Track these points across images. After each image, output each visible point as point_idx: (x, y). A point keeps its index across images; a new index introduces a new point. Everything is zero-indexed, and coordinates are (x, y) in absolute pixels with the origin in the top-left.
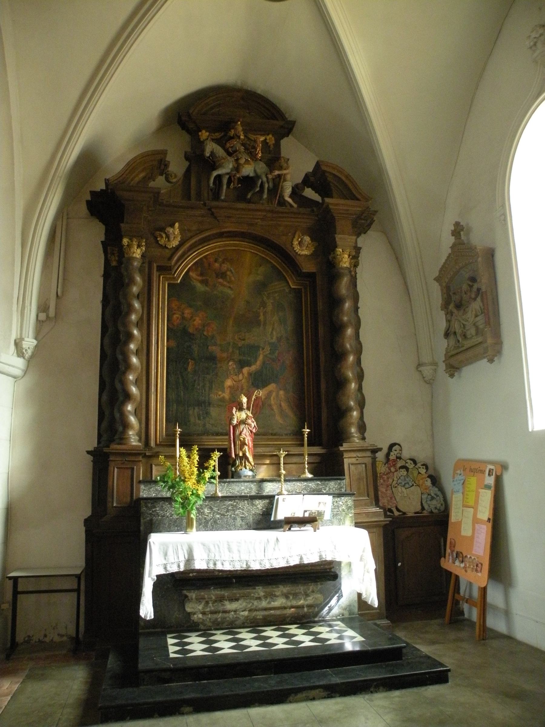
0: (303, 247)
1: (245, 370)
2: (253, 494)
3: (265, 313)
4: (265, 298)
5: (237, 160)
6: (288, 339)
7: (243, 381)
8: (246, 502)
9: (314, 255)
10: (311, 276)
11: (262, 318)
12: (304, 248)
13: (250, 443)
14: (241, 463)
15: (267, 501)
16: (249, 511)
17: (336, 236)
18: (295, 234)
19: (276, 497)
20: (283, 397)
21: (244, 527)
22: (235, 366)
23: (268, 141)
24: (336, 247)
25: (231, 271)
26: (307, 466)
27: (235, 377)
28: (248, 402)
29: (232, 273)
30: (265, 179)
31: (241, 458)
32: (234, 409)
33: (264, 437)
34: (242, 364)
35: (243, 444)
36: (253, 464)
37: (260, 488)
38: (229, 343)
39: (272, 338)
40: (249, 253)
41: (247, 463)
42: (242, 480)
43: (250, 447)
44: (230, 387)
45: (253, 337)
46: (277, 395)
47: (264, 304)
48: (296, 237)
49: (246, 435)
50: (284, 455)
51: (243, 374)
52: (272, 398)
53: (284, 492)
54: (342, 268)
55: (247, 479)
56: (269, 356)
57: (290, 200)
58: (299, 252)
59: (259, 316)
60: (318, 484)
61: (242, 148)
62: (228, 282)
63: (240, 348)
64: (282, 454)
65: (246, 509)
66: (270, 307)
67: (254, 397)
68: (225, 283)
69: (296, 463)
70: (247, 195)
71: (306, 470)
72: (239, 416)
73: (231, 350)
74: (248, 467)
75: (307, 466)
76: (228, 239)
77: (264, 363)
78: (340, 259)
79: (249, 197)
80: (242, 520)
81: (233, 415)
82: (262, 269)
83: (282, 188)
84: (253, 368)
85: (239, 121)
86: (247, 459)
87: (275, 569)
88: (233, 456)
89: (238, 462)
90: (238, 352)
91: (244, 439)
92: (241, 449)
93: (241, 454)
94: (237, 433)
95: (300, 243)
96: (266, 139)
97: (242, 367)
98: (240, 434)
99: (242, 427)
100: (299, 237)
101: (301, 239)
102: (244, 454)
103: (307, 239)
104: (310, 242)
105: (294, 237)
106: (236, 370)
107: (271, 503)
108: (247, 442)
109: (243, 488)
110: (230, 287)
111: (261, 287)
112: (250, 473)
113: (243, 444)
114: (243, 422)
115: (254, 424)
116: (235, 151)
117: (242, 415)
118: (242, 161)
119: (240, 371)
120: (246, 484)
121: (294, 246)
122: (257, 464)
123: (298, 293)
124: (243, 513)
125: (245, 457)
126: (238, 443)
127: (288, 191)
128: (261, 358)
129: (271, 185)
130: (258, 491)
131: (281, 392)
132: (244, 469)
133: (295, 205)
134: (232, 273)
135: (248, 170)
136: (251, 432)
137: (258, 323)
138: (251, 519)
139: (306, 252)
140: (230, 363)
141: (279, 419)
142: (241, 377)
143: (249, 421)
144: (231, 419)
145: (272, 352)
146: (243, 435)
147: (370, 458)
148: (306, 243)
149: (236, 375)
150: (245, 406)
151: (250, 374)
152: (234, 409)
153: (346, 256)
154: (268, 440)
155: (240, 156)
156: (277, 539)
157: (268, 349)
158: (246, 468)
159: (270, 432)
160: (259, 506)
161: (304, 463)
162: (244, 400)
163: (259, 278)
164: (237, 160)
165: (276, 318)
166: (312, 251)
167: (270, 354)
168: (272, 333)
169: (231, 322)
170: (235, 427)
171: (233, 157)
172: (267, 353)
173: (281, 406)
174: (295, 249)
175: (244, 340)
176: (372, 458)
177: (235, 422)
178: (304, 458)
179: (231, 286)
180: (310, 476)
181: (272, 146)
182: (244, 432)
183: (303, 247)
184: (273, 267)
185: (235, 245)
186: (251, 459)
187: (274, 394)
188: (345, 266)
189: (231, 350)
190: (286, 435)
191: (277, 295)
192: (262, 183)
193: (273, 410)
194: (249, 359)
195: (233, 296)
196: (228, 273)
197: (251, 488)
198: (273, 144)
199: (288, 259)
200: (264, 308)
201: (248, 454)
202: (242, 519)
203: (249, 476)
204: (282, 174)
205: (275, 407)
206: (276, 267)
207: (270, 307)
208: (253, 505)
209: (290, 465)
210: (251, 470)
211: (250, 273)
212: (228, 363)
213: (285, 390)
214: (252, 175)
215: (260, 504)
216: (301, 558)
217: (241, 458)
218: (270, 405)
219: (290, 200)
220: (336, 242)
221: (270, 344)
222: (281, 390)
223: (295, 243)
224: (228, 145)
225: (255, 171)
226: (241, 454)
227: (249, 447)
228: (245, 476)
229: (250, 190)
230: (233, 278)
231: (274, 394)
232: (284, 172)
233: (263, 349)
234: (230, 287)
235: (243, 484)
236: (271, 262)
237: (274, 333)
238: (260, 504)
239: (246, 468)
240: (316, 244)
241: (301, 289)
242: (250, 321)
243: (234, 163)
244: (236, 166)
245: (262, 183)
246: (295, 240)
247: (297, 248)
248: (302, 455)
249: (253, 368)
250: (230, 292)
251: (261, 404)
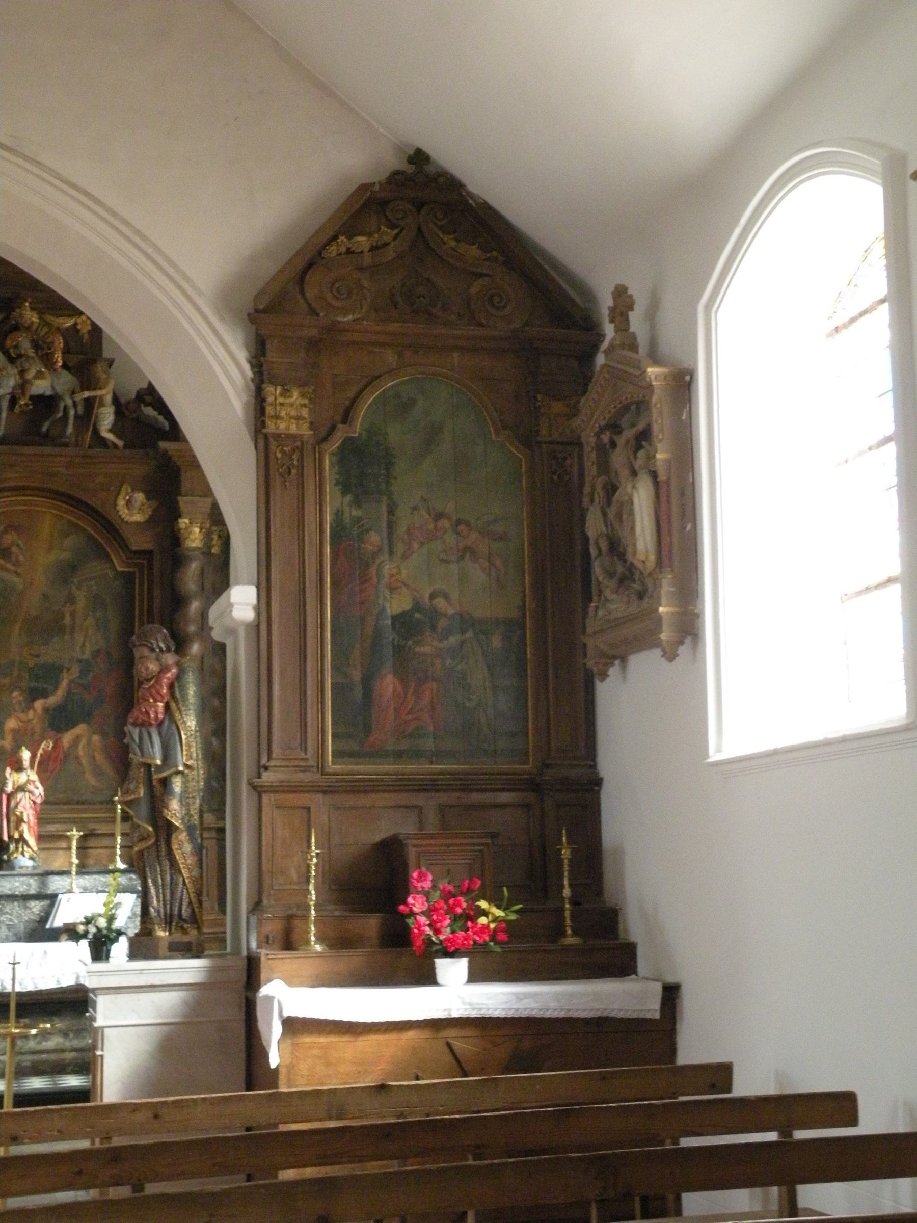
0: (132, 509)
1: (39, 704)
2: (32, 892)
3: (73, 614)
4: (74, 588)
5: (22, 372)
6: (108, 654)
7: (35, 721)
8: (16, 904)
9: (151, 521)
10: (147, 554)
11: (67, 620)
12: (135, 511)
13: (32, 818)
14: (17, 848)
15: (46, 902)
16: (19, 916)
17: (179, 498)
18: (121, 487)
19: (60, 896)
20: (98, 744)
21: (11, 939)
22: (21, 698)
23: (79, 327)
24: (180, 516)
25: (18, 545)
26: (118, 852)
27: (22, 716)
28: (33, 756)
29: (21, 549)
30: (69, 402)
31: (17, 842)
32: (8, 770)
33: (65, 807)
34: (34, 694)
35: (20, 820)
36: (35, 849)
37: (44, 884)
38: (14, 662)
39: (83, 653)
40: (49, 519)
41: (26, 848)
42: (15, 873)
43: (32, 824)
44: (13, 730)
45: (50, 653)
46: (89, 743)
47: (71, 599)
48: (123, 492)
49: (26, 807)
50: (77, 837)
51: (35, 711)
52: (80, 747)
53: (75, 889)
54: (189, 549)
55: (23, 871)
56: (77, 681)
57: (110, 437)
58: (127, 518)
59: (63, 618)
60: (131, 879)
61: (31, 352)
62: (14, 565)
63: (32, 669)
64: (73, 835)
65: (15, 914)
66: (81, 603)
67: (40, 751)
68: (9, 566)
69: (106, 847)
70: (41, 426)
71: (118, 858)
72: (13, 779)
73: (15, 673)
74: (27, 855)
75: (118, 852)
76: (15, 493)
77: (69, 692)
78: (186, 535)
79: (44, 429)
80: (9, 929)
81: (6, 779)
82: (70, 542)
83: (97, 417)
84: (53, 700)
85: (26, 300)
86: (25, 842)
87: (41, 991)
88: (6, 838)
89: (12, 847)
90: (27, 676)
91: (22, 813)
92: (17, 828)
93: (16, 836)
94: (13, 804)
95: (129, 503)
96: (76, 324)
97: (34, 699)
98: (16, 806)
99: (20, 796)
100: (127, 494)
101: (130, 497)
102: (21, 836)
103: (140, 497)
104: (145, 501)
105: (118, 494)
106: (24, 705)
107: (52, 905)
108: (25, 819)
109: (17, 884)
110: (16, 572)
111: (66, 572)
112: (30, 863)
113: (20, 820)
114: (21, 789)
115: (41, 790)
116: (20, 356)
117: (22, 778)
118: (30, 375)
119: (29, 706)
120: (22, 879)
121: (118, 508)
122: (44, 849)
123: (128, 578)
124: (11, 920)
125: (22, 840)
126: (13, 818)
127: (106, 423)
128: (64, 684)
129: (80, 409)
130: (41, 888)
131: (96, 738)
132: (20, 857)
133: (120, 443)
134: (21, 549)
135: (41, 387)
136: (34, 803)
137: (61, 630)
138: (22, 928)
139: (138, 518)
140: (15, 694)
141: (90, 779)
142: (31, 714)
143: (31, 787)
144: (4, 784)
145: (83, 672)
146: (20, 809)
147: (215, 841)
148: (139, 503)
149: (23, 712)
150: (26, 763)
151: (46, 710)
152: (8, 770)
153: (197, 530)
154: (72, 811)
155: (26, 365)
156: (45, 952)
157: (76, 670)
158: (24, 856)
159: (76, 798)
160: (34, 910)
161: (115, 848)
162: (26, 755)
163: (66, 555)
164: (22, 372)
165: (90, 621)
166: (147, 516)
167: (79, 677)
168: (84, 645)
169: (17, 628)
170: (10, 797)
171: (17, 367)
172: (75, 676)
173: (94, 758)
174: (120, 513)
175: (38, 656)
176: (218, 840)
177: (9, 788)
178: (115, 840)
179: (19, 570)
180: (121, 865)
181: (86, 337)
182: (22, 804)
183: (132, 509)
184: (90, 537)
185: (25, 503)
186: (32, 841)
187: (84, 741)
188: (194, 545)
189: (15, 673)
190: (102, 803)
191: (93, 583)
192: (65, 408)
193: (80, 764)
194: (45, 686)
195: (21, 587)
196: (14, 549)
197: (29, 885)
198: (89, 332)
199: (110, 527)
200: (72, 605)
201: (27, 836)
202: (9, 927)
203: (27, 867)
204: (95, 397)
205: (84, 761)
206: (94, 537)
207: (81, 603)
208: (26, 908)
209: (99, 851)
210: (31, 858)
211: (50, 549)
212: (11, 692)
213: (104, 734)
214: (49, 393)
215: (36, 907)
216: (78, 978)
217: (17, 842)
218: (77, 758)
219: (110, 437)
220: (179, 508)
221: (80, 661)
222: (94, 733)
223: (121, 503)
224: (8, 343)
225: (53, 388)
226: (16, 836)
227: (29, 827)
228: (21, 867)
229: (46, 419)
230: (21, 558)
231: (84, 741)
232: (99, 393)
233: (69, 669)
234: (16, 572)
235: (17, 878)
236: (85, 530)
237: (87, 644)
238: (36, 907)
239: (24, 856)
240: (154, 504)
241: (134, 572)
242: (49, 627)
243: (18, 377)
244: (21, 381)
245: (65, 408)
246: (121, 497)
247: (124, 512)
248: (112, 835)
249: (53, 700)
250: (16, 579)
251: (61, 756)
